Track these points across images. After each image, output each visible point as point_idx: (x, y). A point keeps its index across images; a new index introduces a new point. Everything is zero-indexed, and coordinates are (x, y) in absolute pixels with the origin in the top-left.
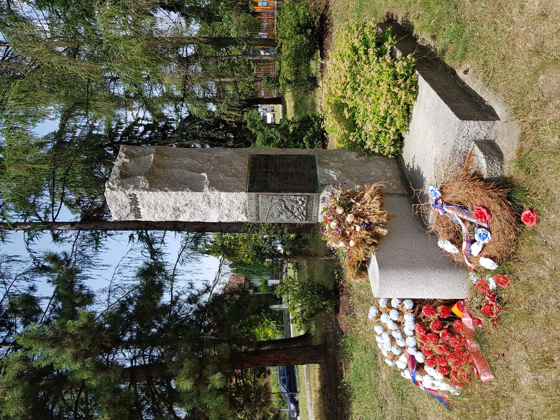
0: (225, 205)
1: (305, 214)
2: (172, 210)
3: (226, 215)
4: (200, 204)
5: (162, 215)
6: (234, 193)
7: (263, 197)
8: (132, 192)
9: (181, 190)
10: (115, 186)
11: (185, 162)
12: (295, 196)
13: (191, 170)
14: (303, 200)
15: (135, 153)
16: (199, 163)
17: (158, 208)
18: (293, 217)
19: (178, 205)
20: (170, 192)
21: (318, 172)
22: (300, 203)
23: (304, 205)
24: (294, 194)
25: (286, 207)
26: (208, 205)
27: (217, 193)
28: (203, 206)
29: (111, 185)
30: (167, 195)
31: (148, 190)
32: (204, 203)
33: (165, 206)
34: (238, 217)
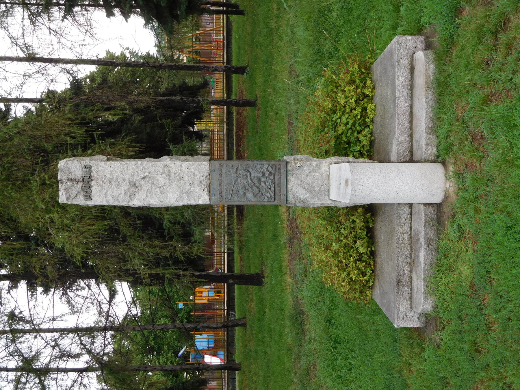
1: (273, 189)
2: (128, 184)
3: (187, 193)
17: (113, 183)
18: (260, 193)
22: (267, 174)
23: (272, 177)
25: (251, 180)
26: (167, 178)
28: (161, 180)
32: (164, 175)
33: (120, 180)
34: (199, 198)
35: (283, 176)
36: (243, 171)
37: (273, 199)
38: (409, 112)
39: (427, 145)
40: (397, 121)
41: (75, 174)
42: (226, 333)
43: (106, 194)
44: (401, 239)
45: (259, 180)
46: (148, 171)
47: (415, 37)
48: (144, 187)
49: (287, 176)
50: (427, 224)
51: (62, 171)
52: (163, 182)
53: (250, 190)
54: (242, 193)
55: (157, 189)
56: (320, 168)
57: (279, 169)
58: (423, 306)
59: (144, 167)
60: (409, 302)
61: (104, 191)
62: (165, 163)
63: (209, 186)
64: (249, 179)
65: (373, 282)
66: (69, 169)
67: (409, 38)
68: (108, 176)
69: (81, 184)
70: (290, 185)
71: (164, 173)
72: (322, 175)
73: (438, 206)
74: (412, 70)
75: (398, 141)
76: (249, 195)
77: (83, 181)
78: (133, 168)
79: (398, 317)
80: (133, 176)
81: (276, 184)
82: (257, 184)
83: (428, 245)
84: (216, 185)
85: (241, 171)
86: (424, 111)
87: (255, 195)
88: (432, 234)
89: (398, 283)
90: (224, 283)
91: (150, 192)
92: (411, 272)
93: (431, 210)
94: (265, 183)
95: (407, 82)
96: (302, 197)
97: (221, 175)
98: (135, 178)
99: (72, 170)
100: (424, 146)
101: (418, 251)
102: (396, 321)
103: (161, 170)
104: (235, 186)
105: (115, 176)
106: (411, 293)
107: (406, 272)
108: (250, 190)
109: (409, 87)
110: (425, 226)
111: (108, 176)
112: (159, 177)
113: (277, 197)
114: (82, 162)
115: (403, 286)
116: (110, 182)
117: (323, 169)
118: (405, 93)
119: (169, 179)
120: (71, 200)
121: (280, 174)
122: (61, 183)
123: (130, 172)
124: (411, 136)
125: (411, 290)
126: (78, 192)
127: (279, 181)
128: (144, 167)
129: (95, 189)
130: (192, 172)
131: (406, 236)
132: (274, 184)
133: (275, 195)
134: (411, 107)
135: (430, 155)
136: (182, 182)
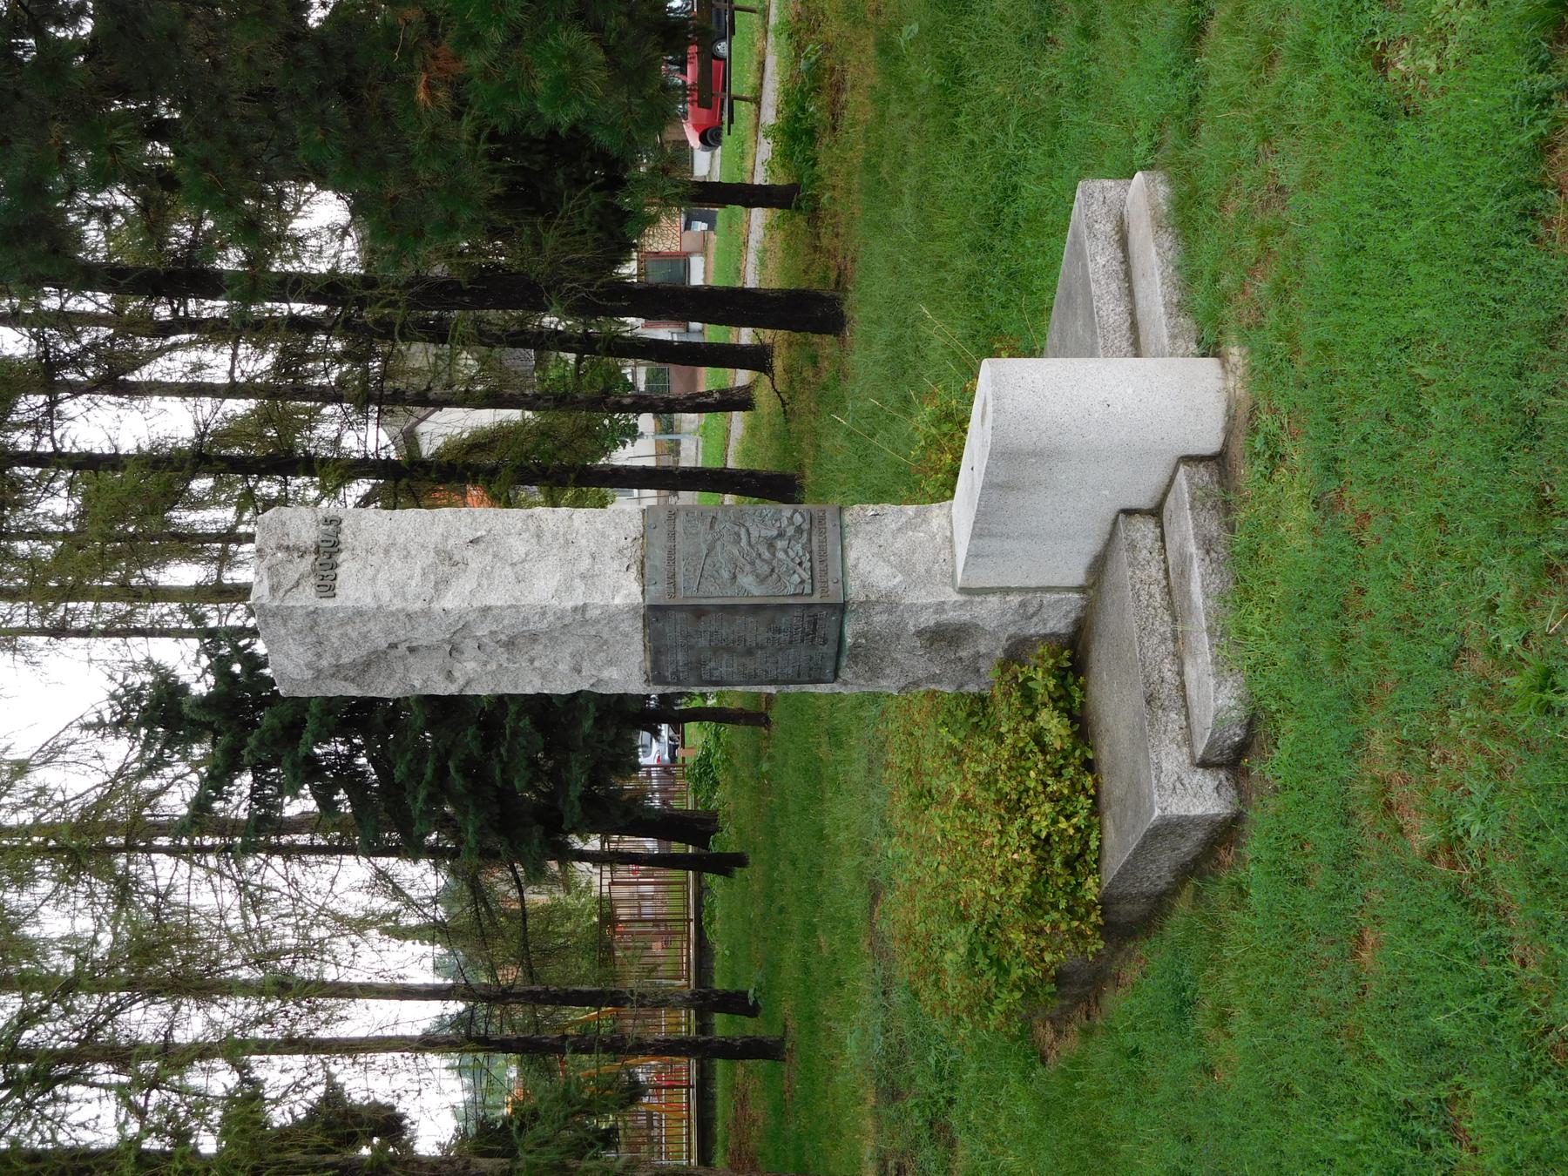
1: (807, 565)
2: (432, 554)
3: (583, 577)
22: (790, 531)
28: (519, 547)
32: (526, 535)
34: (616, 590)
37: (808, 590)
41: (298, 538)
43: (374, 579)
44: (1144, 597)
46: (486, 527)
48: (473, 565)
50: (1198, 504)
52: (522, 551)
53: (748, 568)
54: (726, 575)
55: (508, 568)
57: (822, 519)
58: (1216, 699)
59: (474, 519)
60: (1185, 750)
61: (370, 571)
63: (642, 562)
64: (744, 543)
65: (1100, 840)
66: (284, 524)
67: (1108, 183)
68: (383, 540)
69: (311, 558)
70: (852, 556)
71: (528, 530)
72: (933, 537)
73: (1219, 461)
74: (1123, 242)
76: (747, 581)
77: (317, 551)
78: (447, 522)
79: (1160, 786)
80: (446, 538)
82: (766, 555)
83: (1208, 552)
84: (659, 556)
87: (762, 580)
88: (1213, 527)
89: (1148, 703)
90: (688, 869)
91: (489, 576)
93: (1203, 475)
94: (786, 552)
96: (883, 585)
97: (672, 535)
98: (451, 542)
99: (291, 528)
101: (1184, 574)
102: (1156, 797)
104: (709, 561)
105: (401, 540)
106: (1188, 726)
107: (1168, 675)
109: (1122, 276)
110: (1192, 508)
112: (513, 541)
113: (818, 585)
116: (387, 552)
117: (935, 524)
118: (1114, 287)
120: (281, 593)
121: (822, 533)
123: (440, 531)
125: (1187, 717)
126: (302, 576)
127: (822, 549)
128: (474, 519)
129: (347, 567)
131: (1155, 589)
132: (811, 553)
136: (571, 550)
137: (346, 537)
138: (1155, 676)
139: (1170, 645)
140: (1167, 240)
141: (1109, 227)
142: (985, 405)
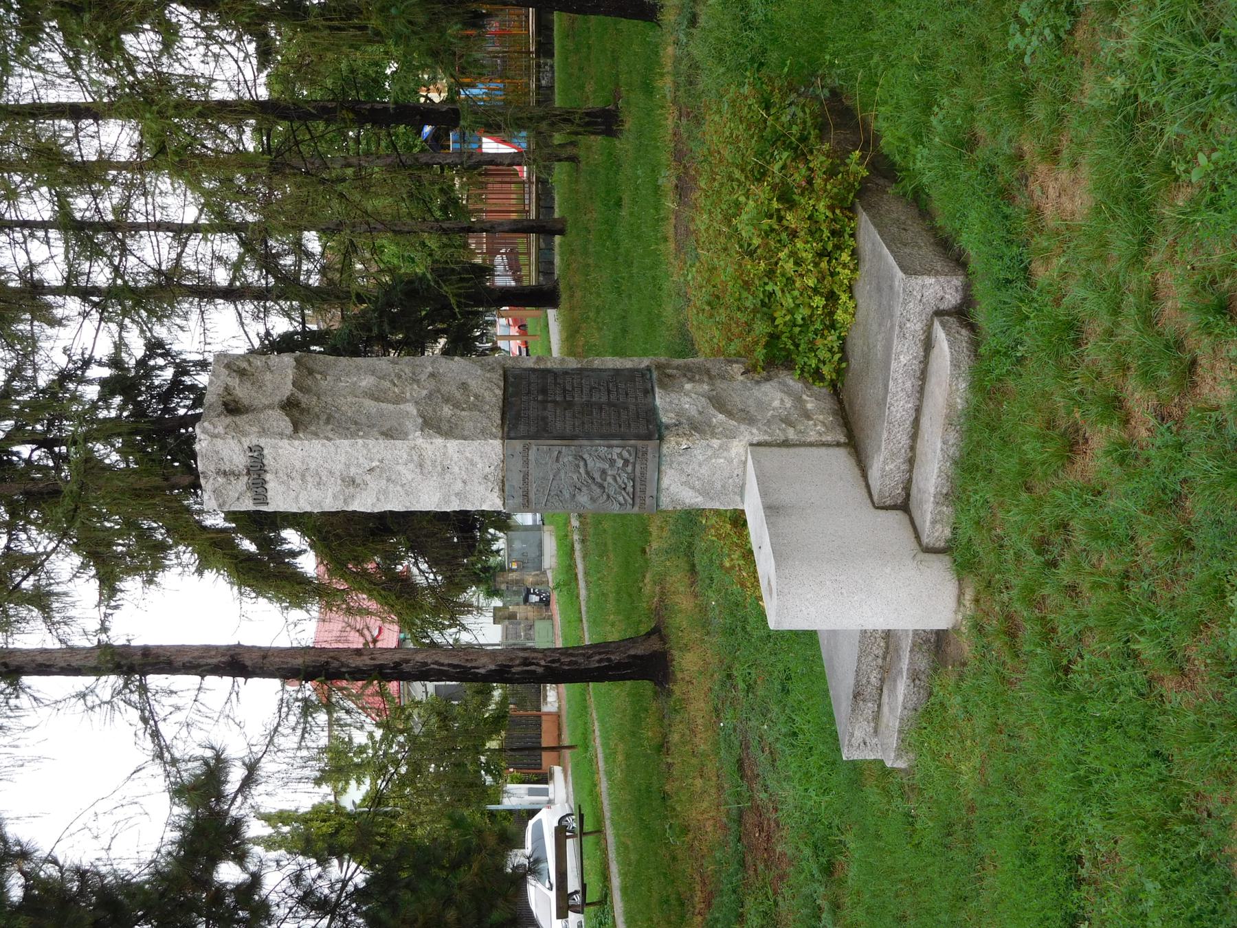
0: (456, 469)
1: (630, 489)
2: (339, 482)
3: (457, 495)
4: (400, 468)
5: (316, 494)
6: (476, 443)
7: (537, 450)
8: (255, 442)
9: (362, 437)
10: (220, 430)
11: (364, 383)
12: (609, 446)
13: (377, 399)
14: (625, 454)
15: (248, 368)
16: (395, 385)
17: (309, 479)
18: (605, 497)
19: (353, 471)
20: (338, 442)
21: (658, 402)
22: (620, 463)
23: (629, 469)
24: (606, 442)
25: (587, 473)
26: (418, 470)
27: (439, 441)
28: (407, 473)
29: (211, 427)
30: (332, 449)
31: (290, 437)
32: (411, 466)
33: (324, 474)
34: (483, 501)
35: (651, 465)
36: (570, 458)
38: (911, 419)
39: (934, 522)
40: (885, 436)
42: (533, 244)
43: (297, 497)
45: (604, 472)
46: (379, 456)
47: (942, 279)
48: (371, 485)
49: (659, 465)
51: (205, 456)
53: (584, 489)
55: (399, 488)
56: (727, 449)
57: (645, 453)
61: (293, 494)
62: (412, 443)
64: (582, 470)
67: (930, 280)
70: (665, 482)
71: (412, 461)
75: (883, 470)
77: (248, 473)
80: (348, 466)
81: (637, 479)
84: (516, 480)
85: (567, 459)
86: (937, 466)
92: (882, 680)
95: (916, 366)
100: (928, 523)
103: (405, 456)
105: (313, 465)
107: (873, 680)
108: (584, 489)
109: (918, 374)
111: (298, 465)
113: (638, 500)
114: (243, 439)
115: (864, 701)
116: (303, 477)
118: (908, 384)
119: (422, 473)
122: (205, 477)
124: (911, 461)
129: (272, 485)
130: (467, 458)
133: (633, 499)
134: (918, 410)
135: (938, 539)
137: (268, 461)
138: (864, 681)
139: (880, 661)
140: (953, 437)
141: (919, 326)
142: (769, 583)
